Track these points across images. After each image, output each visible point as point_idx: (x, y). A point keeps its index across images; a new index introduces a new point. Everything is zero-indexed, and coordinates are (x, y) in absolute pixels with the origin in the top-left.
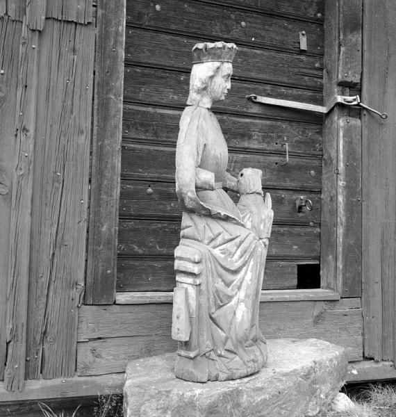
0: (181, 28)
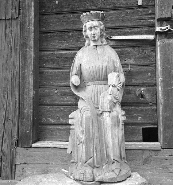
0: (69, 9)
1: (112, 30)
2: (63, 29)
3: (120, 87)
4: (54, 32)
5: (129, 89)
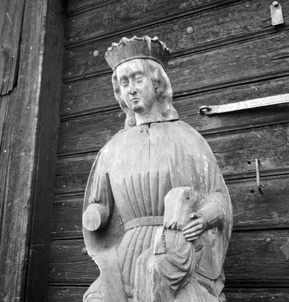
1: (214, 92)
2: (105, 105)
3: (194, 229)
4: (88, 114)
5: (265, 241)
